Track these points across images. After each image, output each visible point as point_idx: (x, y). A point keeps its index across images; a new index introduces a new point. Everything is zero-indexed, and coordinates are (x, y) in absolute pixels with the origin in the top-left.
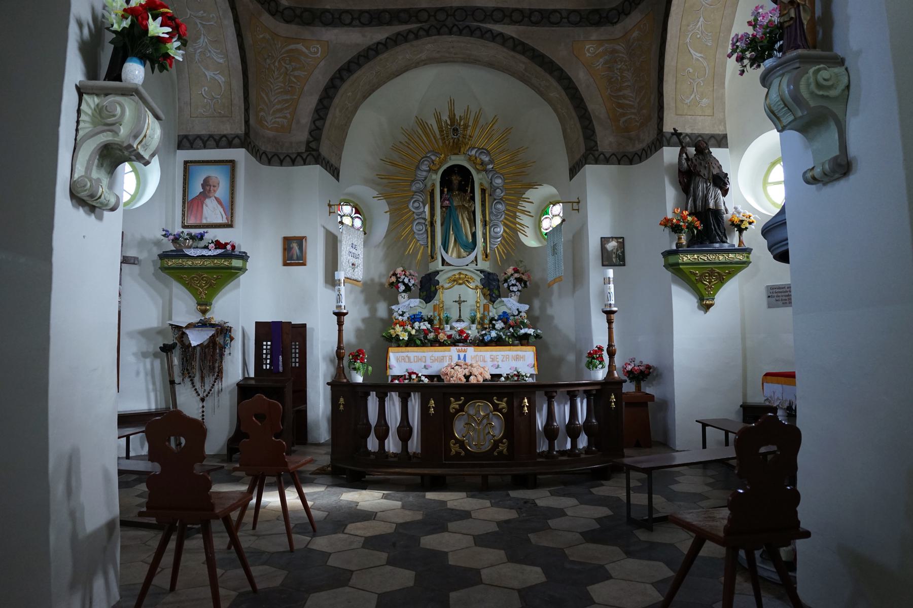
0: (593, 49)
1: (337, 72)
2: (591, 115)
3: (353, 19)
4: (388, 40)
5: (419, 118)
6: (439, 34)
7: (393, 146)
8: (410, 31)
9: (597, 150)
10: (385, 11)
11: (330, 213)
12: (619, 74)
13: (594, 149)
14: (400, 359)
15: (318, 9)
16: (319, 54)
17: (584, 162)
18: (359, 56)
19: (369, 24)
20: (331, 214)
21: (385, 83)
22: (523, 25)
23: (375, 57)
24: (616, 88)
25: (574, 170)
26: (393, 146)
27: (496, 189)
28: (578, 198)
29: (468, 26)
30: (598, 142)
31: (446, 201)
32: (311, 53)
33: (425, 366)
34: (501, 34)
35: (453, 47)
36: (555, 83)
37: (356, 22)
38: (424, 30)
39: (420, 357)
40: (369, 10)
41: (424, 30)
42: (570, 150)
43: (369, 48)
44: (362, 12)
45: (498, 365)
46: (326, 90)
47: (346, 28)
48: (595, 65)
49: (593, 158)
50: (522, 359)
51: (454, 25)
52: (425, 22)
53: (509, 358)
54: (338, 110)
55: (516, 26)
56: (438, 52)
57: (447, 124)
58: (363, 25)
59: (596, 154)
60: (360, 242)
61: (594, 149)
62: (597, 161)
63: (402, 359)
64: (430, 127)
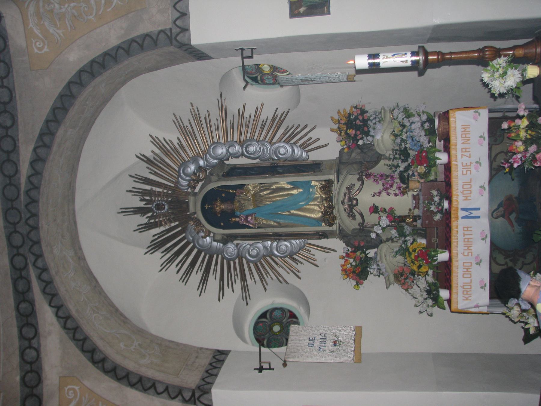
0: (38, 43)
1: (96, 365)
2: (125, 40)
3: (30, 347)
4: (52, 304)
5: (147, 250)
6: (38, 242)
7: (183, 282)
8: (39, 277)
9: (171, 29)
10: (17, 309)
11: (270, 369)
12: (66, 6)
13: (169, 34)
14: (467, 296)
15: (21, 391)
16: (77, 388)
17: (187, 47)
18: (74, 339)
19: (35, 328)
20: (272, 367)
21: (106, 297)
22: (18, 135)
23: (74, 320)
24: (86, 9)
25: (199, 55)
26: (183, 282)
27: (230, 153)
28: (237, 50)
29: (26, 206)
30: (160, 28)
31: (249, 220)
32: (76, 396)
33: (477, 264)
34: (32, 163)
35: (55, 220)
36: (89, 89)
37: (34, 343)
38: (36, 261)
39: (465, 270)
40: (18, 327)
41: (36, 261)
42: (172, 61)
43: (65, 327)
44: (22, 336)
45: (477, 162)
46: (119, 379)
47: (43, 355)
48: (59, 38)
49: (181, 35)
50: (468, 130)
51: (26, 223)
52: (26, 259)
53: (466, 149)
54: (143, 361)
55: (20, 145)
56: (63, 237)
57: (152, 216)
58: (36, 334)
59: (175, 30)
60: (303, 332)
61: (169, 34)
62: (185, 30)
63: (467, 294)
64: (156, 237)
